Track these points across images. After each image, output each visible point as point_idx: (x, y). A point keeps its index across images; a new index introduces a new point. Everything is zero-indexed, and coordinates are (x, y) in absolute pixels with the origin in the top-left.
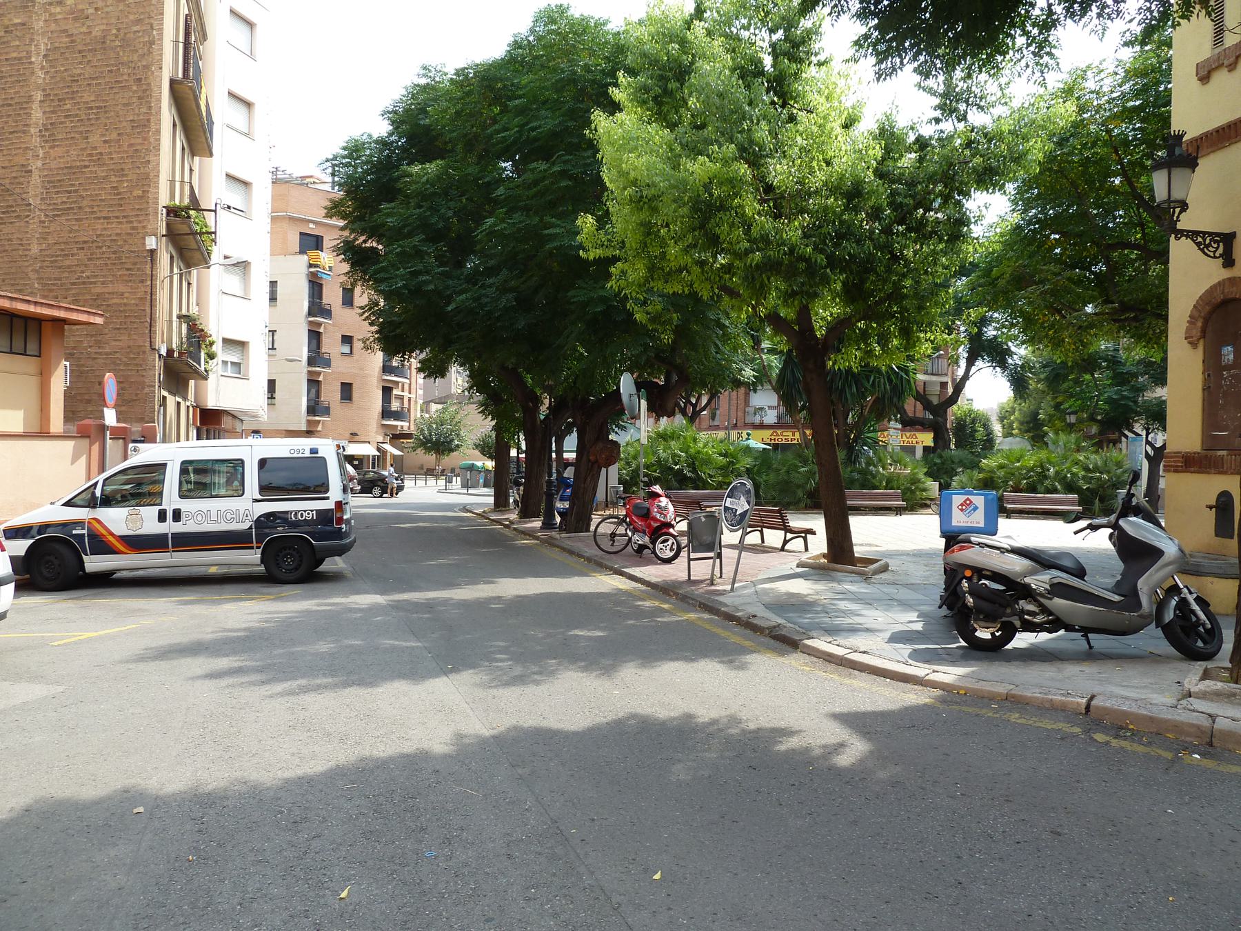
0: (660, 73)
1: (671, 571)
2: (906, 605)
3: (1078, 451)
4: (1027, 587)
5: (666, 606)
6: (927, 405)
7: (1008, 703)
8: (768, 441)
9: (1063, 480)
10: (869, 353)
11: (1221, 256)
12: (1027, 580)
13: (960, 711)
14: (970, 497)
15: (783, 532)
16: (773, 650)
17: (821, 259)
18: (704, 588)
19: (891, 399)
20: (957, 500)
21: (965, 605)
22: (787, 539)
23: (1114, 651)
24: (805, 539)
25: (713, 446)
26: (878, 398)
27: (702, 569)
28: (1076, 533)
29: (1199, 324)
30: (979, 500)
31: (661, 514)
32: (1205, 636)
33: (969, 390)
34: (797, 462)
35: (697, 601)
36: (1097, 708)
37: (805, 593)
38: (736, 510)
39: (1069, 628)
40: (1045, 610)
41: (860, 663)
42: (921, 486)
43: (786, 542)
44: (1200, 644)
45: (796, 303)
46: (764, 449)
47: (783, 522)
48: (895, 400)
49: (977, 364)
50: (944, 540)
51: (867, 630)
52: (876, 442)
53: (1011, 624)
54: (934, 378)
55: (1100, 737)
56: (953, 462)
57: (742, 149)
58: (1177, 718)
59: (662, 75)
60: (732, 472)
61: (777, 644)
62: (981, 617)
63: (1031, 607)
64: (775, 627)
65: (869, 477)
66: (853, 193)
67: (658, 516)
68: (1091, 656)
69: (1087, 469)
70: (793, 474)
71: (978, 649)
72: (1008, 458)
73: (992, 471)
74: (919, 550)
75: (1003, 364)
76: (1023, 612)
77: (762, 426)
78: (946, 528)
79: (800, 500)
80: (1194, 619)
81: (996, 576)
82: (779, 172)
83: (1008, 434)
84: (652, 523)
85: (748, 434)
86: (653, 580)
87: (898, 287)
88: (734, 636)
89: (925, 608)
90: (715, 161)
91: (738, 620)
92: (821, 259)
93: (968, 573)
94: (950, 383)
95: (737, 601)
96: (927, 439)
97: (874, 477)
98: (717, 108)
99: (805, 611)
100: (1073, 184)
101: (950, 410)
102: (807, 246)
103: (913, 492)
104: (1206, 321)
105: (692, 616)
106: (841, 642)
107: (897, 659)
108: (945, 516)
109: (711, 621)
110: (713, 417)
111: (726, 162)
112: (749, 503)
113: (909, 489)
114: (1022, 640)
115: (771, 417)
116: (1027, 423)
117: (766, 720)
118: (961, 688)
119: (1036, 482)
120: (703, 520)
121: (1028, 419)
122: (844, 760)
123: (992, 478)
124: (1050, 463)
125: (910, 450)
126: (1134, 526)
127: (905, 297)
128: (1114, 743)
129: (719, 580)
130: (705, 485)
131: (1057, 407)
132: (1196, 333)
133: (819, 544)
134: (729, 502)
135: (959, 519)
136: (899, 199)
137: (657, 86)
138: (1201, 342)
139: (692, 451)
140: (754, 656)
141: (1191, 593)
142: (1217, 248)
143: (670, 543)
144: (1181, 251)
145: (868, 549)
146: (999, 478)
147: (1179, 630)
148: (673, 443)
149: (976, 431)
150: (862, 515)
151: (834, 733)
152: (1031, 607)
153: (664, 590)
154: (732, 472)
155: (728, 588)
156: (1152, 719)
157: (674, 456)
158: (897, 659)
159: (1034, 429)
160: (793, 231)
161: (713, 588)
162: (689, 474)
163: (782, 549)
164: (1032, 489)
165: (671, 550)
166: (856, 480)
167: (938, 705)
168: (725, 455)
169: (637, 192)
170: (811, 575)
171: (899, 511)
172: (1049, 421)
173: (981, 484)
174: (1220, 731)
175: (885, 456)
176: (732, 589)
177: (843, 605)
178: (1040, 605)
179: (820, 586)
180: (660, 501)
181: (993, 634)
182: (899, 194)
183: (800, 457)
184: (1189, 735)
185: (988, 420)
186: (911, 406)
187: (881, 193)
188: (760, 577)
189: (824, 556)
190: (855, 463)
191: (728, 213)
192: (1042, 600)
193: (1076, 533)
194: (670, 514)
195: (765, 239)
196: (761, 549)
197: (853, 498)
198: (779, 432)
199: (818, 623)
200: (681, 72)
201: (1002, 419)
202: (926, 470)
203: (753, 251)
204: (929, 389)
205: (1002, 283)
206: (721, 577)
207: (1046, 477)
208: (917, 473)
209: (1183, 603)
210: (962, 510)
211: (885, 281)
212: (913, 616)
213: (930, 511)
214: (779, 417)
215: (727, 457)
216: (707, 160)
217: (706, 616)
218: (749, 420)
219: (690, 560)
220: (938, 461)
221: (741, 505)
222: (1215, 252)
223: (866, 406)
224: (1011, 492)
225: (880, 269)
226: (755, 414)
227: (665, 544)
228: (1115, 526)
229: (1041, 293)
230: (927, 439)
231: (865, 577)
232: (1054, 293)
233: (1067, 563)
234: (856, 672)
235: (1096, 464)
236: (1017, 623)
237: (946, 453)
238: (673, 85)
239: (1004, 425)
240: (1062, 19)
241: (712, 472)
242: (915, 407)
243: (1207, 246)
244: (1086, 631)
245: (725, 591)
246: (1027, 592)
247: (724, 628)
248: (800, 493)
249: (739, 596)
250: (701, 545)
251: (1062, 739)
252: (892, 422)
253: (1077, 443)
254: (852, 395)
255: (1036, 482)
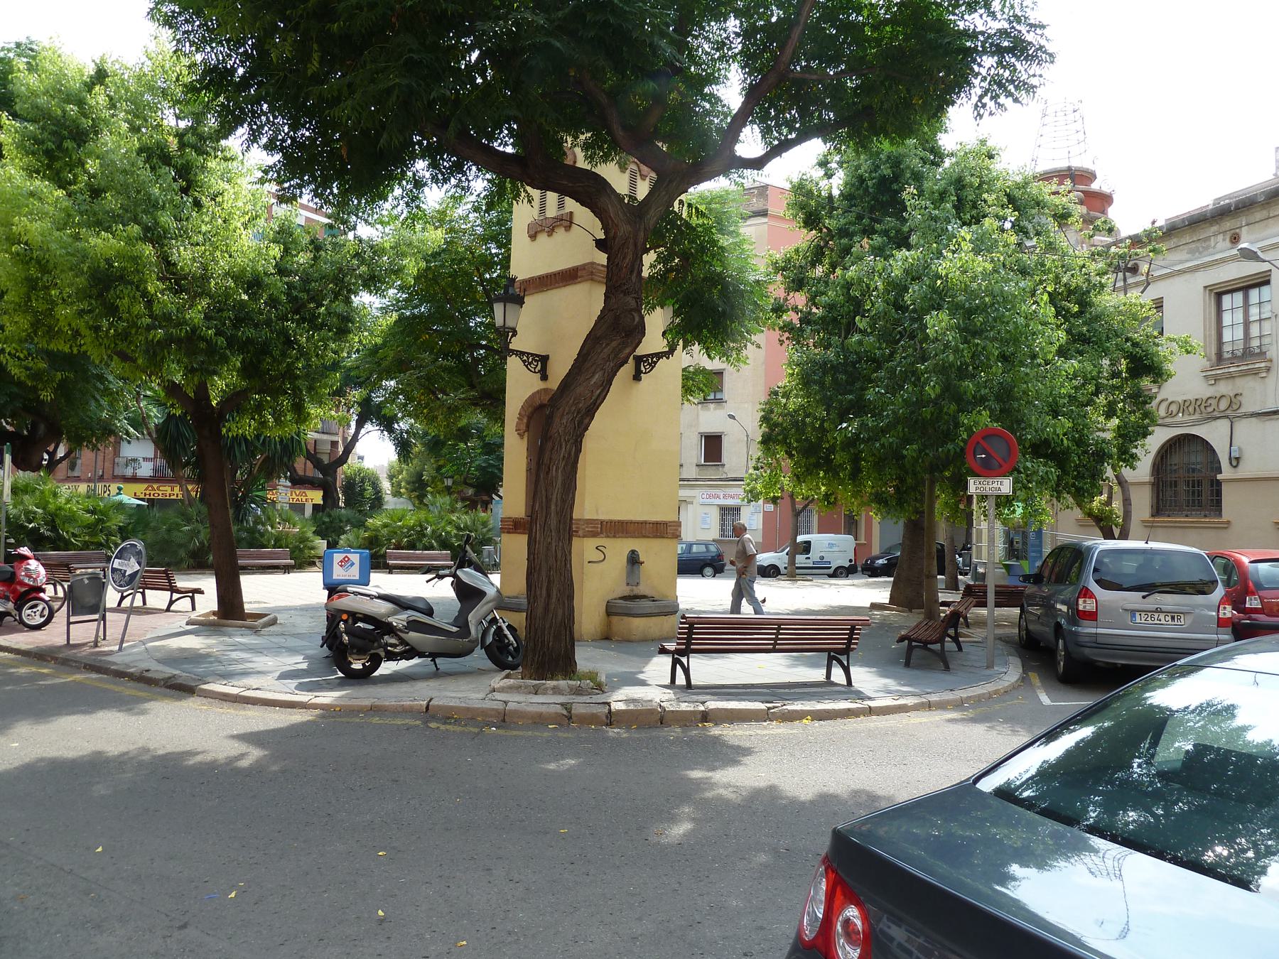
0: (54, 128)
1: (44, 637)
2: (293, 651)
3: (453, 512)
4: (390, 624)
5: (45, 671)
6: (317, 464)
7: (372, 712)
8: (142, 496)
9: (438, 538)
10: (263, 424)
11: (539, 371)
12: (390, 619)
13: (335, 721)
14: (349, 555)
15: (169, 593)
16: (172, 697)
17: (221, 341)
18: (86, 650)
19: (281, 459)
20: (338, 557)
21: (342, 643)
22: (174, 599)
23: (454, 670)
24: (193, 599)
25: (78, 502)
26: (268, 457)
27: (84, 632)
28: (427, 582)
29: (525, 421)
30: (355, 558)
31: (30, 577)
32: (514, 653)
33: (359, 448)
34: (179, 521)
35: (81, 663)
36: (434, 706)
37: (198, 647)
38: (125, 571)
39: (421, 655)
40: (403, 642)
41: (253, 698)
42: (309, 544)
43: (171, 602)
44: (510, 659)
45: (196, 379)
46: (138, 505)
47: (169, 582)
48: (285, 459)
49: (366, 426)
50: (326, 592)
51: (259, 672)
52: (264, 500)
53: (378, 655)
54: (325, 437)
55: (433, 725)
56: (341, 521)
57: (146, 229)
58: (484, 706)
59: (56, 131)
60: (101, 531)
61: (173, 692)
62: (355, 651)
63: (393, 641)
64: (170, 678)
65: (257, 535)
66: (254, 284)
67: (26, 581)
68: (437, 674)
69: (458, 528)
70: (175, 533)
71: (354, 678)
72: (391, 519)
73: (377, 530)
74: (306, 605)
75: (391, 430)
76: (387, 644)
77: (134, 479)
78: (328, 581)
79: (182, 560)
80: (506, 641)
81: (367, 618)
82: (184, 255)
83: (396, 494)
84: (18, 588)
85: (120, 489)
86: (24, 647)
87: (291, 367)
88: (128, 689)
89: (310, 652)
90: (118, 238)
91: (131, 677)
92: (221, 341)
93: (345, 617)
94: (340, 442)
95: (127, 659)
96: (316, 497)
97: (262, 535)
98: (121, 185)
99: (198, 662)
100: (444, 291)
101: (339, 470)
102: (208, 328)
103: (301, 550)
104: (530, 418)
105: (79, 677)
106: (235, 683)
107: (287, 691)
108: (327, 573)
109: (100, 680)
110: (72, 467)
111: (130, 241)
112: (139, 564)
113: (298, 547)
114: (386, 668)
115: (146, 470)
116: (413, 483)
117: (169, 747)
118: (337, 706)
119: (415, 539)
120: (86, 582)
121: (414, 479)
122: (244, 763)
123: (376, 537)
124: (428, 522)
125: (298, 508)
126: (467, 575)
127: (297, 377)
128: (443, 727)
129: (104, 642)
130: (67, 546)
131: (439, 469)
132: (523, 427)
133: (209, 602)
134: (117, 563)
135: (339, 574)
136: (295, 293)
137: (50, 141)
138: (526, 434)
139: (51, 507)
140: (152, 703)
141: (504, 622)
142: (537, 366)
143: (40, 608)
144: (513, 364)
145: (256, 606)
146: (383, 536)
147: (496, 649)
148: (26, 498)
149: (365, 490)
150: (249, 574)
151: (237, 748)
152: (393, 641)
153: (40, 656)
154: (101, 531)
155: (117, 648)
156: (468, 709)
157: (27, 513)
158: (287, 691)
159: (418, 488)
160: (196, 314)
161: (97, 649)
162: (48, 533)
163: (168, 610)
164: (412, 546)
165: (42, 616)
166: (243, 539)
167: (318, 719)
168: (93, 512)
169: (26, 250)
170: (202, 631)
171: (287, 569)
172: (433, 482)
173: (367, 543)
174: (510, 711)
175: (274, 515)
176: (120, 649)
177: (234, 655)
178: (400, 638)
179: (212, 641)
180: (28, 564)
181: (363, 665)
182: (295, 288)
183: (183, 515)
184: (491, 716)
185: (378, 479)
186: (302, 465)
187: (279, 284)
188: (148, 637)
189: (214, 613)
190: (242, 521)
191: (129, 287)
192: (400, 634)
193: (427, 582)
194: (41, 578)
195: (167, 317)
196: (145, 611)
197: (244, 557)
198: (155, 486)
199: (212, 671)
200: (81, 136)
201: (391, 477)
202: (314, 529)
203: (155, 328)
204: (320, 448)
205: (385, 364)
206: (104, 639)
207: (424, 535)
208: (305, 532)
209: (500, 628)
210: (341, 566)
211: (280, 363)
212: (300, 658)
213: (315, 569)
214: (155, 470)
215: (95, 514)
216: (110, 236)
217: (94, 676)
218: (118, 472)
219: (69, 623)
220: (327, 520)
221: (132, 566)
222: (535, 368)
223: (255, 464)
224: (393, 549)
225: (276, 353)
226: (127, 466)
227: (34, 610)
228: (454, 576)
229: (418, 378)
230: (316, 497)
231: (255, 631)
232: (428, 378)
233: (421, 605)
234: (249, 706)
235: (466, 523)
236: (383, 654)
237: (335, 512)
238: (69, 144)
239: (393, 484)
240: (430, 182)
241: (76, 531)
242: (305, 463)
243: (530, 364)
244: (434, 656)
245: (112, 651)
246: (389, 629)
247: (115, 684)
248: (182, 553)
249: (129, 655)
250: (83, 607)
251: (408, 729)
252: (282, 480)
253: (452, 505)
254: (241, 453)
255: (415, 539)
